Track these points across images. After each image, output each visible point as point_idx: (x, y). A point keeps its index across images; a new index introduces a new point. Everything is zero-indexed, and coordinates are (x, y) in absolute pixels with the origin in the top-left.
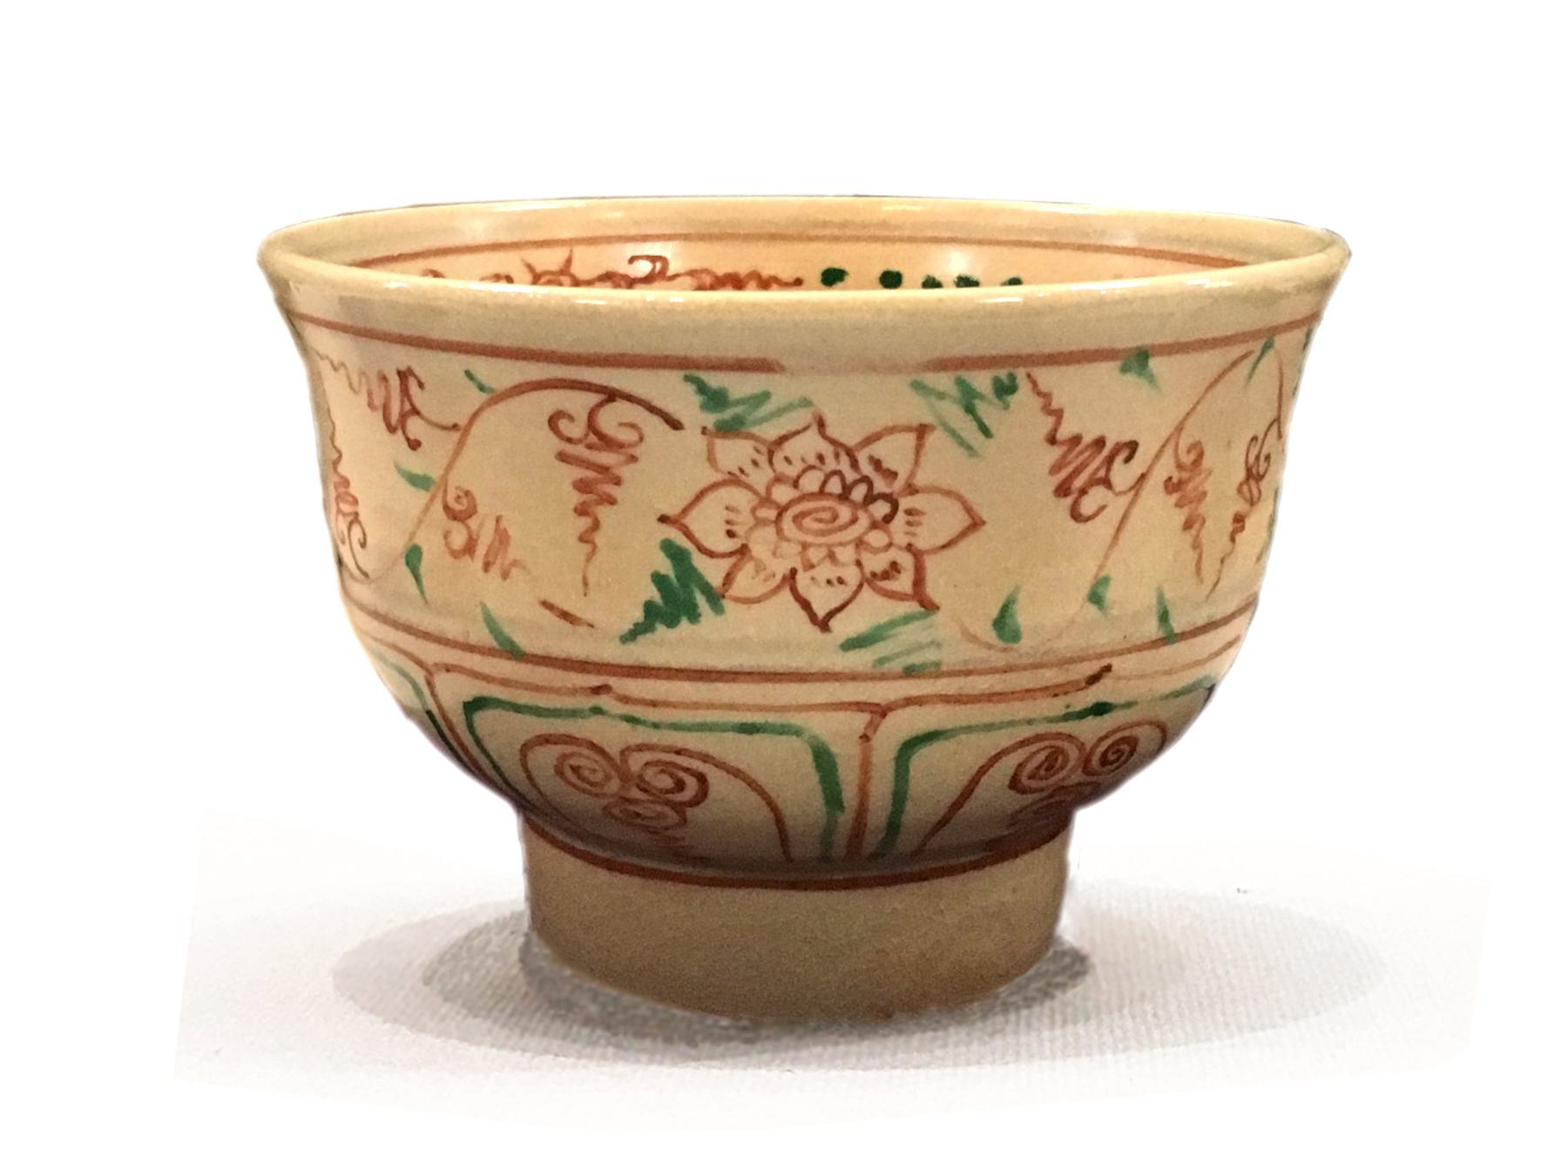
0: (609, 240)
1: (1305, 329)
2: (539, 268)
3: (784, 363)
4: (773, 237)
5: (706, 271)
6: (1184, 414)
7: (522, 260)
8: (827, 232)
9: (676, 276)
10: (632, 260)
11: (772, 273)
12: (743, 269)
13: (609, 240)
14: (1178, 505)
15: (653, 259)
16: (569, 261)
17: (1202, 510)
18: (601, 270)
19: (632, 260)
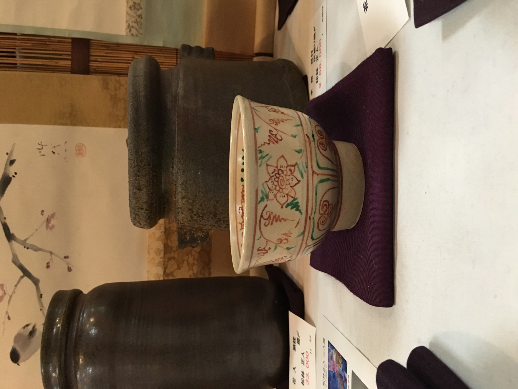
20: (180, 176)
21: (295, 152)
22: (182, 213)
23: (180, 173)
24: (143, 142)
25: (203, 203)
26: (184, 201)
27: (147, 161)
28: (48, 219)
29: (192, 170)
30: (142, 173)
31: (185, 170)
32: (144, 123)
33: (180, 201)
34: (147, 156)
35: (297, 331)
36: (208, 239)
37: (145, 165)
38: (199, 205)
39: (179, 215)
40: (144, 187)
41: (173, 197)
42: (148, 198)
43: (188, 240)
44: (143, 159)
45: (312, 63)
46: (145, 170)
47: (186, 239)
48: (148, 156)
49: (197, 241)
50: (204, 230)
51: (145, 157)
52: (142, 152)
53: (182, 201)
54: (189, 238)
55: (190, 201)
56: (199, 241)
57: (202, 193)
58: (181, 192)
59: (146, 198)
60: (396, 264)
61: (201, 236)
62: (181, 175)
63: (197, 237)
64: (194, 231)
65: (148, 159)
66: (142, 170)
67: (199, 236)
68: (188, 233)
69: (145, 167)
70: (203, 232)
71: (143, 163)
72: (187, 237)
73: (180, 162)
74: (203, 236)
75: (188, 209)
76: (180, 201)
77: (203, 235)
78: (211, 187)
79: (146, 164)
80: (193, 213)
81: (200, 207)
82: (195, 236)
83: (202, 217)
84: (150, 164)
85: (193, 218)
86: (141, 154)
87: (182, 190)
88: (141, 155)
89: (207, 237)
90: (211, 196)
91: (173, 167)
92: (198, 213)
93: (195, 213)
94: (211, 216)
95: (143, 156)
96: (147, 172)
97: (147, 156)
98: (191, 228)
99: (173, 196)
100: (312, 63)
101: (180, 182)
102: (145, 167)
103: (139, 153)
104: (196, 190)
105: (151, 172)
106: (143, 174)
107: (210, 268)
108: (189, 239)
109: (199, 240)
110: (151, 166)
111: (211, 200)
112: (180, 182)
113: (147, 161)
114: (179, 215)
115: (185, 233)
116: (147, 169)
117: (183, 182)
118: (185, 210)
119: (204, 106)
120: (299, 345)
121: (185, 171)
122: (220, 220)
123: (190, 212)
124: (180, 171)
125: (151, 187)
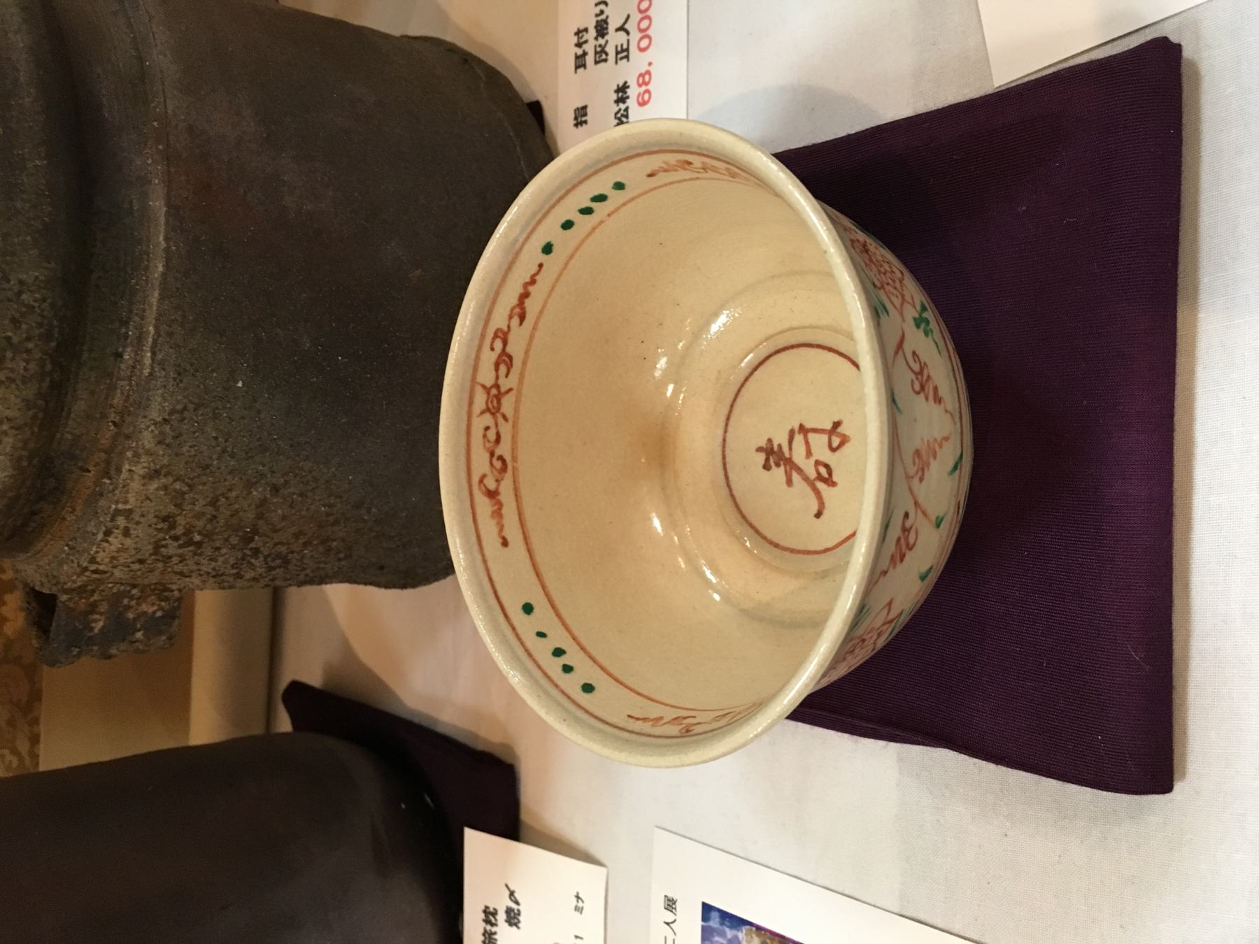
0: (477, 358)
1: (860, 631)
2: (484, 407)
3: (479, 418)
4: (509, 268)
5: (512, 309)
6: (790, 344)
7: (478, 416)
8: (521, 240)
9: (509, 326)
10: (492, 349)
11: (529, 276)
12: (520, 290)
13: (477, 358)
14: (495, 933)
15: (496, 336)
16: (483, 386)
17: (650, 87)
18: (492, 368)
19: (492, 349)
20: (160, 391)
21: (890, 314)
22: (126, 533)
23: (165, 377)
24: (29, 238)
25: (223, 495)
26: (154, 485)
27: (39, 319)
28: (823, 578)
29: (213, 371)
30: (12, 370)
31: (188, 367)
32: (38, 163)
33: (135, 485)
34: (44, 300)
35: (507, 886)
36: (177, 622)
37: (28, 339)
38: (209, 500)
39: (107, 541)
40: (12, 428)
41: (90, 471)
42: (10, 477)
43: (96, 630)
44: (24, 309)
45: (616, 63)
46: (25, 356)
47: (92, 629)
48: (49, 301)
49: (133, 634)
50: (172, 591)
51: (36, 304)
52: (21, 282)
53: (144, 485)
54: (101, 624)
55: (178, 486)
56: (139, 635)
57: (232, 456)
58: (149, 453)
59: (6, 474)
60: (1186, 658)
61: (154, 612)
62: (165, 387)
63: (135, 619)
64: (132, 598)
65: (45, 313)
66: (13, 359)
67: (145, 613)
68: (103, 607)
69: (30, 345)
70: (167, 599)
71: (24, 326)
72: (96, 621)
73: (170, 334)
74: (159, 614)
75: (156, 517)
76: (135, 485)
77: (161, 608)
78: (270, 434)
79: (37, 332)
80: (173, 532)
81: (210, 510)
82: (131, 615)
83: (199, 545)
84: (47, 337)
85: (162, 550)
86: (16, 288)
87: (160, 443)
88: (20, 293)
89: (174, 618)
90: (261, 468)
91: (119, 356)
92: (188, 531)
93: (179, 531)
94: (234, 540)
95: (24, 297)
96: (33, 366)
97: (44, 300)
98: (122, 588)
99: (91, 468)
100: (616, 63)
101: (154, 414)
102: (30, 345)
103: (12, 283)
104: (214, 447)
105: (49, 367)
106: (12, 375)
107: (36, 721)
108: (103, 627)
109: (139, 630)
110: (53, 344)
111: (256, 483)
112: (154, 414)
113: (39, 319)
114: (107, 541)
115: (93, 608)
116: (38, 355)
117: (169, 414)
118: (142, 520)
119: (265, 135)
120: (518, 928)
121: (185, 370)
122: (256, 552)
123: (159, 530)
124: (164, 369)
125: (36, 430)
